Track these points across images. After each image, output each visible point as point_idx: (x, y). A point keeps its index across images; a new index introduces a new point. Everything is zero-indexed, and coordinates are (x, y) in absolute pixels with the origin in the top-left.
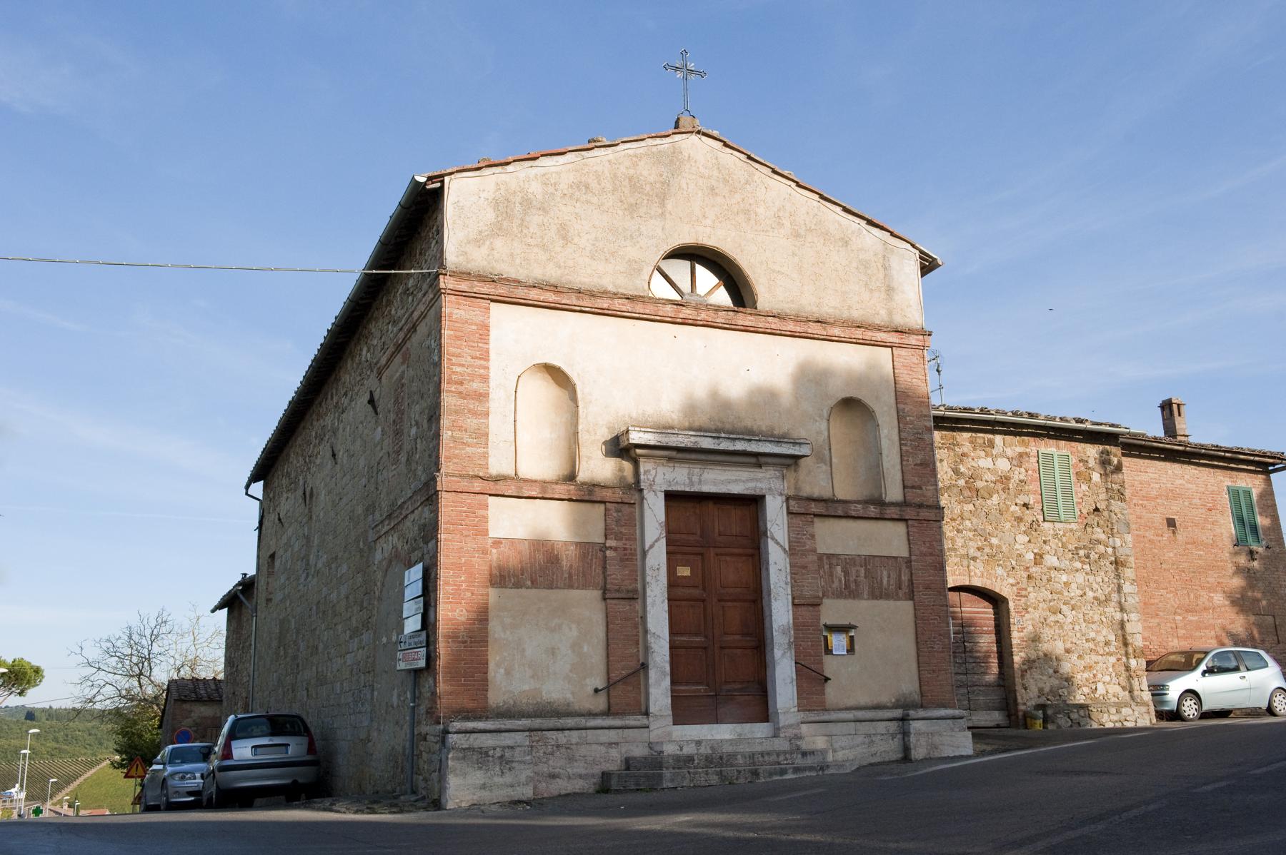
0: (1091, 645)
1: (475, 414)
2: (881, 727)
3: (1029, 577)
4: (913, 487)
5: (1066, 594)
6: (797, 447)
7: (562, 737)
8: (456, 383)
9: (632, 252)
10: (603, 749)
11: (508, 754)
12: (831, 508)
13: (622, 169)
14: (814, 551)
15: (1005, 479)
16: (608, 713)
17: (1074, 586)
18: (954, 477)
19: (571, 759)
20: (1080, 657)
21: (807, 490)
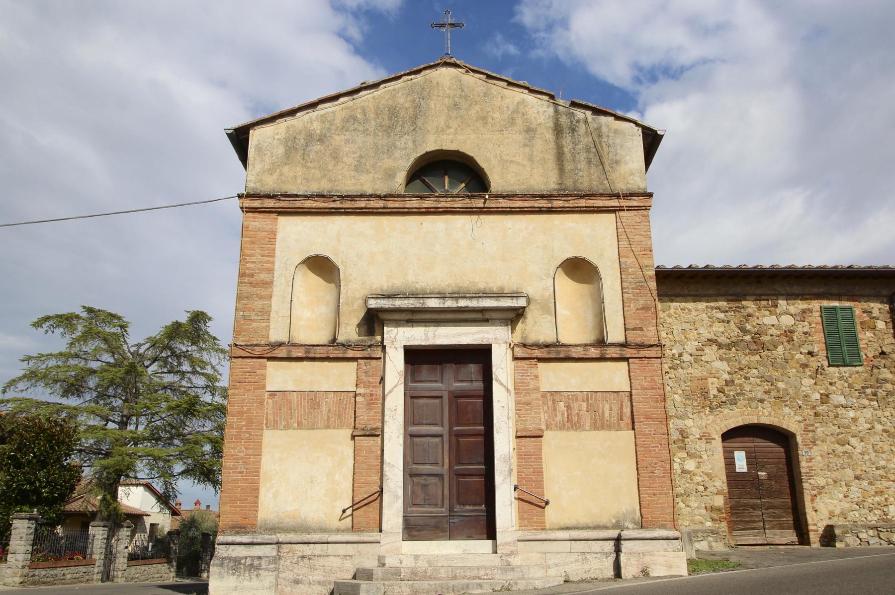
0: (881, 472)
1: (261, 297)
2: (596, 546)
3: (816, 415)
4: (634, 329)
5: (853, 428)
6: (515, 300)
7: (307, 550)
8: (249, 276)
9: (388, 163)
10: (339, 560)
11: (256, 563)
12: (555, 353)
13: (383, 102)
14: (537, 389)
15: (789, 333)
16: (353, 529)
17: (861, 421)
18: (741, 334)
19: (313, 568)
20: (871, 483)
21: (532, 338)
